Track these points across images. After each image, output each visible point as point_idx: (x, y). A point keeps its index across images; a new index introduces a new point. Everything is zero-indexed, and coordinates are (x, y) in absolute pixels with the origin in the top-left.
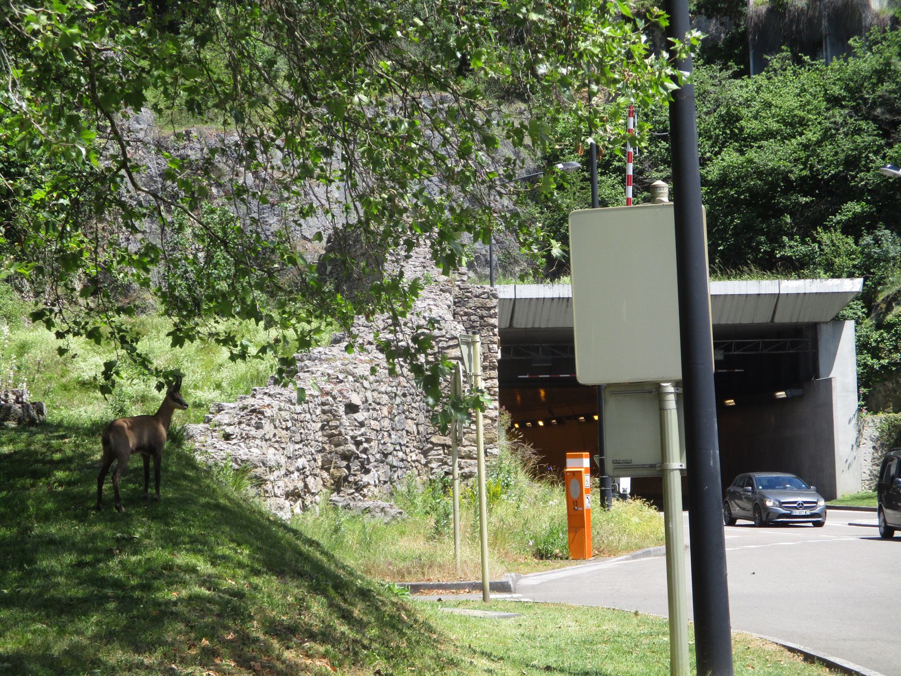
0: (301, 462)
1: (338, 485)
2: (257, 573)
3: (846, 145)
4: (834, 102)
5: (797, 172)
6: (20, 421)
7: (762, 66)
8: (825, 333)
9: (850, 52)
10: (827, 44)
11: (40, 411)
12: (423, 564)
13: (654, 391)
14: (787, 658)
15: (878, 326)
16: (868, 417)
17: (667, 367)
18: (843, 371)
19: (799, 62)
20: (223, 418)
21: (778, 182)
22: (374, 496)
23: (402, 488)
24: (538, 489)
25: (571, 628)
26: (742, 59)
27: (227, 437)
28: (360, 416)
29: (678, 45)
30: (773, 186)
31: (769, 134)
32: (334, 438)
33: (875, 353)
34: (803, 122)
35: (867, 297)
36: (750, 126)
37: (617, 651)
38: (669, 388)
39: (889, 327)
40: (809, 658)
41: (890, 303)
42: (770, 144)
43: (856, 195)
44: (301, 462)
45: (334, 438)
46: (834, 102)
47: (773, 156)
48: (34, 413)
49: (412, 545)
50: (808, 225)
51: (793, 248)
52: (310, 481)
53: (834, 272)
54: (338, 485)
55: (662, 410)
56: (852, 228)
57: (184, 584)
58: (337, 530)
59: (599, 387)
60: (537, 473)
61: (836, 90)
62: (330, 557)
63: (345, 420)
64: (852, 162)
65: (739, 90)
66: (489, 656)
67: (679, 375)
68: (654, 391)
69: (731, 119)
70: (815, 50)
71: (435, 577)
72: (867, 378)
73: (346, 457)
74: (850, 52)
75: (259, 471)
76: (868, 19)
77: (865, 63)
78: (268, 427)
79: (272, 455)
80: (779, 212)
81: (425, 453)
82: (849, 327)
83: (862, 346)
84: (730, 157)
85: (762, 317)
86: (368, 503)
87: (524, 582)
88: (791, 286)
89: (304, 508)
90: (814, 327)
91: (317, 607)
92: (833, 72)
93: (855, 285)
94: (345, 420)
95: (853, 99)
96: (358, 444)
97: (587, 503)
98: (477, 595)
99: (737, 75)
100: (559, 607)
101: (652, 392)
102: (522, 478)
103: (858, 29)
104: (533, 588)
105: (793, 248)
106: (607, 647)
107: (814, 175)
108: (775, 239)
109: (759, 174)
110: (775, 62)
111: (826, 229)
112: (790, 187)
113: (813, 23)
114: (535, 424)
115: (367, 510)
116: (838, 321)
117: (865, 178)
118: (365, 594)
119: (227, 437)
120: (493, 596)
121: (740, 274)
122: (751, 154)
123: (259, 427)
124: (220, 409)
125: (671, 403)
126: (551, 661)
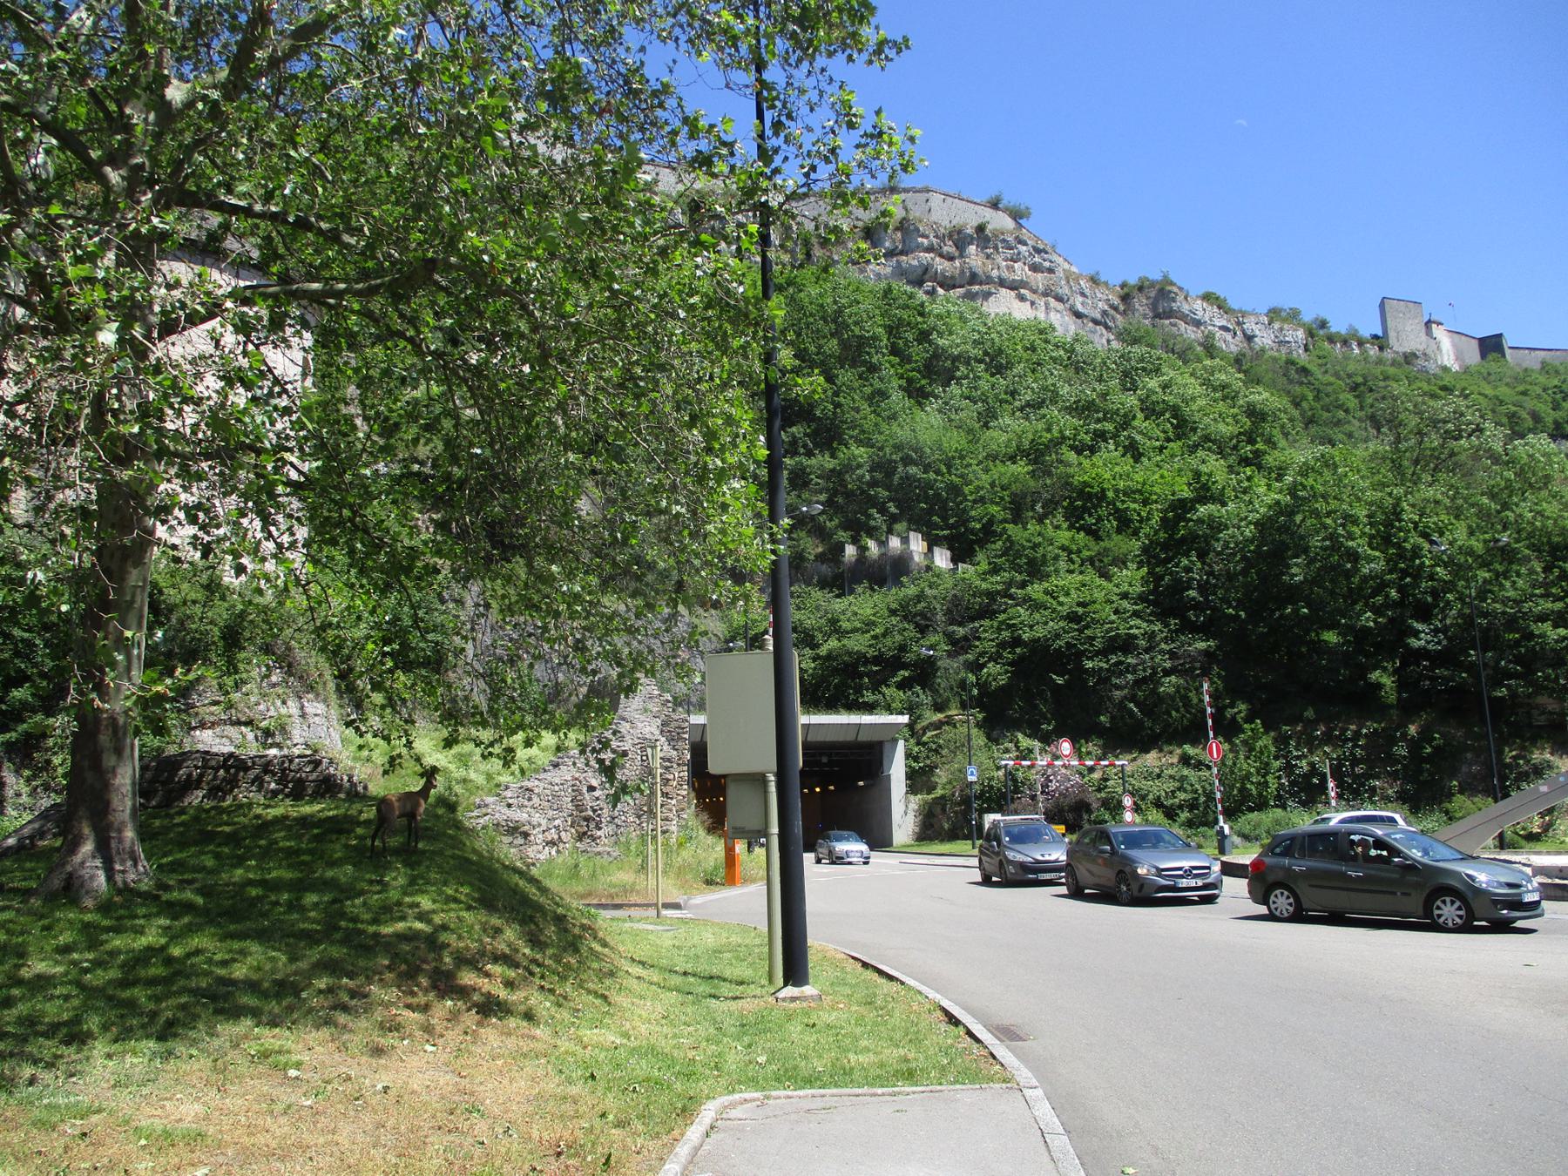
0: (557, 823)
1: (581, 837)
2: (469, 908)
3: (898, 638)
4: (893, 612)
5: (871, 653)
6: (348, 794)
7: (852, 591)
8: (887, 747)
9: (902, 585)
10: (889, 580)
11: (365, 788)
12: (626, 889)
13: (761, 779)
14: (851, 966)
15: (918, 744)
16: (912, 797)
17: (766, 762)
18: (897, 770)
19: (873, 590)
20: (508, 794)
21: (861, 658)
22: (604, 845)
23: (623, 839)
24: (710, 839)
25: (709, 939)
26: (841, 587)
27: (509, 806)
28: (597, 793)
29: (775, 529)
30: (858, 660)
31: (855, 630)
32: (579, 807)
33: (916, 759)
34: (874, 623)
35: (911, 726)
36: (845, 625)
37: (737, 958)
38: (772, 778)
39: (924, 744)
40: (865, 965)
41: (925, 730)
42: (857, 636)
43: (905, 666)
44: (557, 823)
45: (579, 807)
46: (893, 612)
47: (858, 643)
48: (360, 789)
49: (624, 877)
50: (878, 683)
51: (869, 697)
52: (563, 834)
53: (889, 709)
54: (581, 837)
55: (766, 792)
56: (901, 686)
57: (403, 918)
58: (576, 866)
59: (724, 776)
60: (711, 830)
61: (894, 606)
62: (544, 890)
63: (587, 796)
64: (903, 648)
65: (839, 605)
66: (642, 963)
67: (775, 769)
68: (761, 779)
69: (834, 622)
70: (882, 582)
71: (634, 899)
72: (912, 775)
73: (587, 819)
74: (902, 585)
75: (526, 828)
76: (913, 566)
77: (912, 591)
78: (536, 800)
79: (537, 818)
80: (861, 676)
81: (639, 817)
82: (901, 743)
83: (908, 755)
84: (833, 643)
85: (850, 737)
86: (600, 849)
87: (693, 902)
88: (867, 719)
89: (558, 852)
90: (881, 744)
91: (511, 934)
92: (892, 596)
93: (905, 719)
94: (587, 796)
95: (904, 611)
96: (594, 811)
97: (737, 849)
98: (652, 912)
99: (838, 596)
100: (705, 922)
101: (759, 780)
102: (702, 833)
103: (907, 573)
104: (697, 906)
105: (869, 697)
106: (728, 955)
107: (881, 654)
108: (859, 691)
109: (849, 653)
110: (859, 589)
111: (888, 686)
112: (867, 661)
113: (881, 568)
114: (812, 790)
115: (599, 853)
116: (895, 741)
117: (909, 657)
118: (560, 920)
119: (509, 806)
120: (664, 912)
121: (837, 712)
122: (845, 641)
123: (530, 799)
124: (507, 788)
125: (773, 788)
126: (689, 967)
